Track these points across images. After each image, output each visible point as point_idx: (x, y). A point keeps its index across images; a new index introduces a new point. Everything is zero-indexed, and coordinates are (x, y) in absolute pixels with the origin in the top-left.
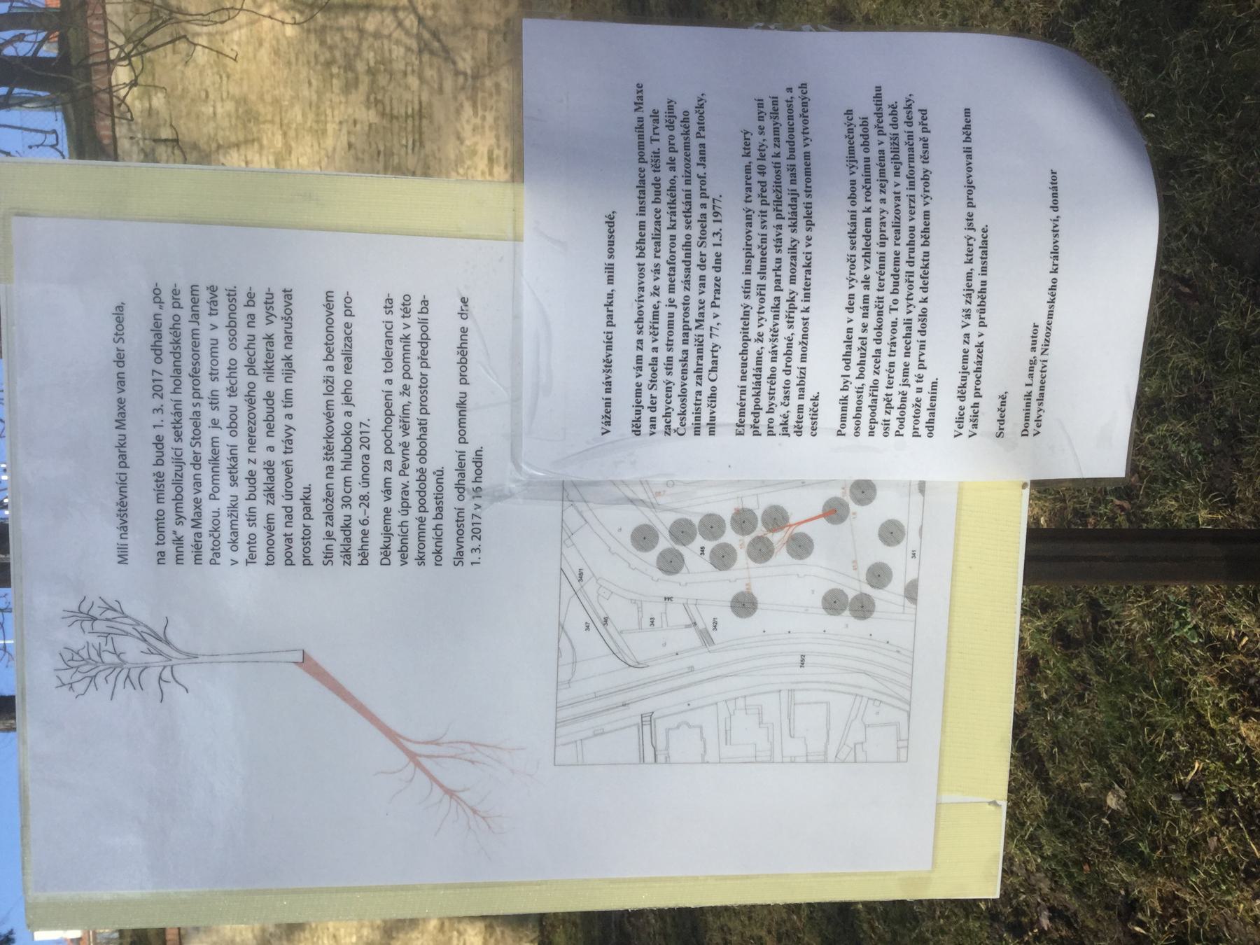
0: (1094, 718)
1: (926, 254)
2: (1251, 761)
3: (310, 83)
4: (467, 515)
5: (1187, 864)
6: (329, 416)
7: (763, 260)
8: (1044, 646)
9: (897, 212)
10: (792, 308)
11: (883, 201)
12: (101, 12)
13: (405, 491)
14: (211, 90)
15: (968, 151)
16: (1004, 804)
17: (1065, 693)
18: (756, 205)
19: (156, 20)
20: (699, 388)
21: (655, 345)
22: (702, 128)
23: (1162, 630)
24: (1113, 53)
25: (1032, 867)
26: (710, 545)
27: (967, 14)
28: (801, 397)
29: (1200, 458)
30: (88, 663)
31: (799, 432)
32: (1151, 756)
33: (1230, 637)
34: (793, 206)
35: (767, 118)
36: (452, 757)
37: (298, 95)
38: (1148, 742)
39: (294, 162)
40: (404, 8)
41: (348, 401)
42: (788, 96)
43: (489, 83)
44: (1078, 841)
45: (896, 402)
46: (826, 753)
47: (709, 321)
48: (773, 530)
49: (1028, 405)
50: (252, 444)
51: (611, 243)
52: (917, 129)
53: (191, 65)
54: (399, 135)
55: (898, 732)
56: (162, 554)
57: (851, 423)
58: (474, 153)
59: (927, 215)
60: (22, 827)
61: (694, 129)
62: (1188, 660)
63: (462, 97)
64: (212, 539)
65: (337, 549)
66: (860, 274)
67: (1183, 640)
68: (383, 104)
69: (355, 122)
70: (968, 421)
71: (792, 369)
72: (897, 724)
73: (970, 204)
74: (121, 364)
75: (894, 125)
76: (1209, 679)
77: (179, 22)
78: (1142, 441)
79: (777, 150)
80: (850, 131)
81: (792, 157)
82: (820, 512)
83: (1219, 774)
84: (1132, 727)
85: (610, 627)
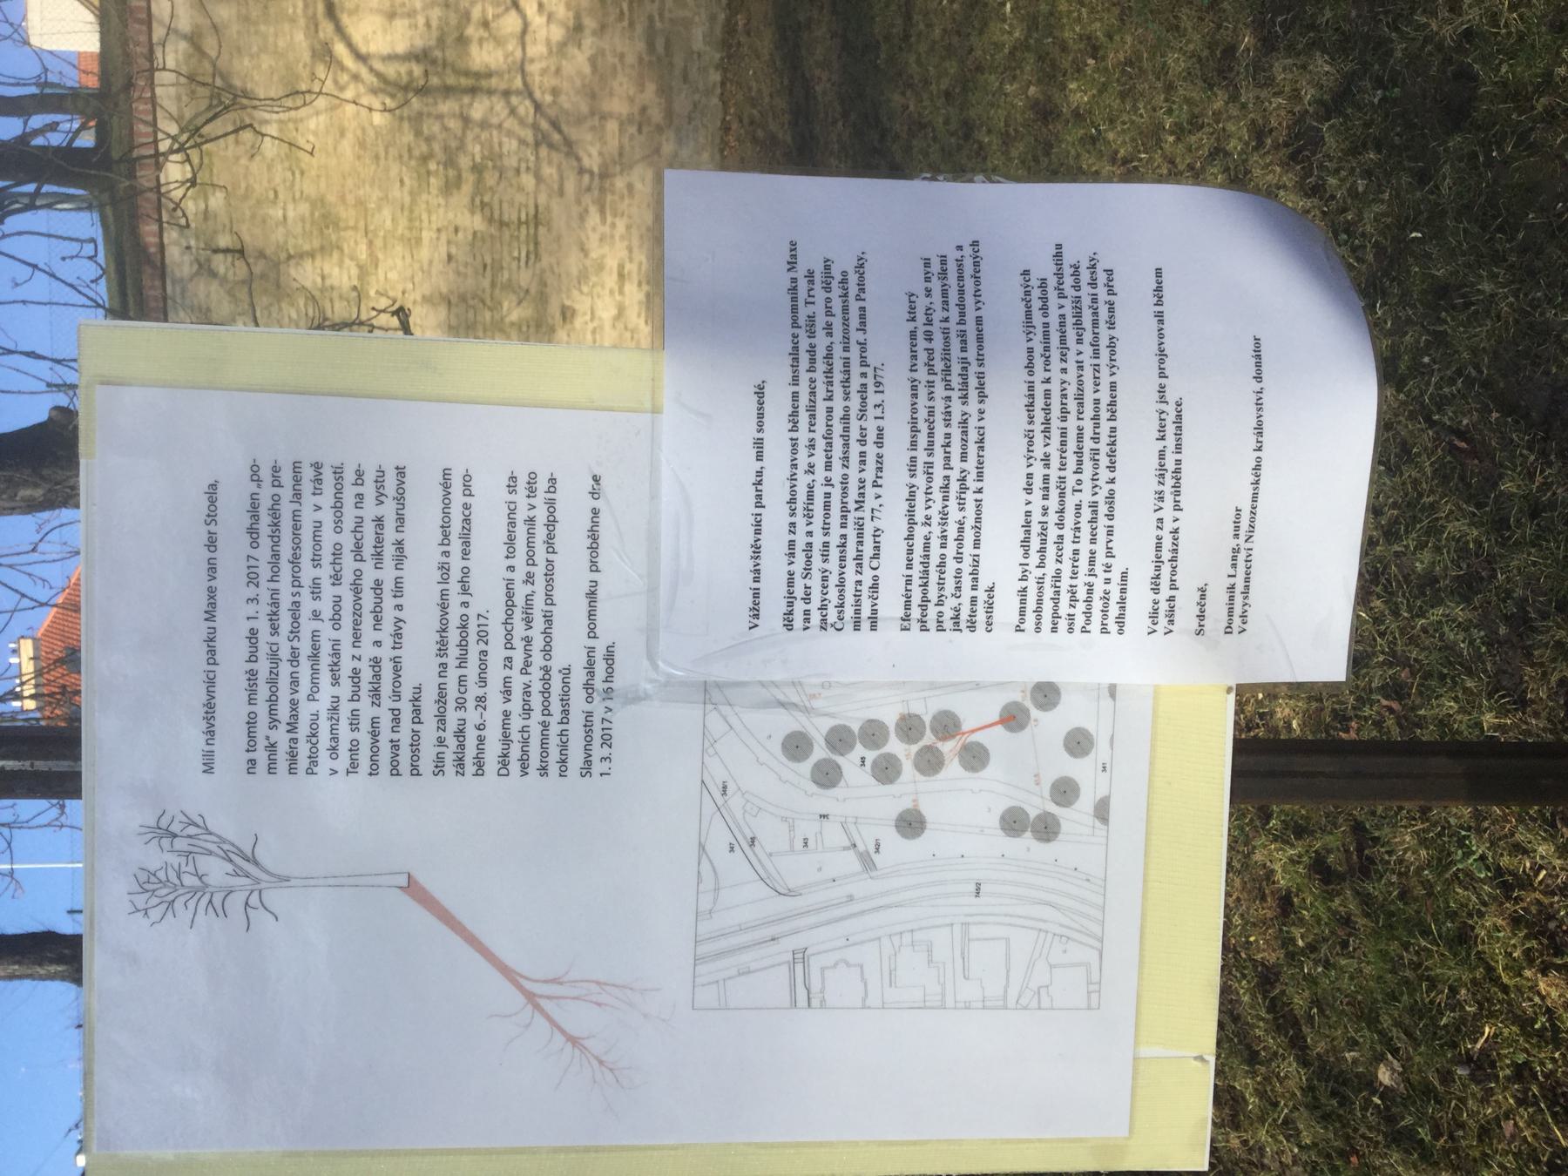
0: (1361, 971)
1: (1113, 429)
2: (1553, 1025)
3: (402, 181)
4: (596, 719)
5: (1477, 1154)
6: (444, 607)
7: (931, 435)
8: (1299, 881)
9: (1080, 383)
10: (964, 488)
11: (1064, 370)
12: (149, 95)
13: (527, 692)
14: (281, 190)
15: (1160, 317)
16: (1212, 1060)
17: (1325, 940)
18: (922, 374)
19: (217, 106)
20: (859, 577)
21: (809, 528)
22: (862, 290)
23: (1442, 862)
24: (1372, 160)
25: (1287, 1159)
26: (870, 756)
27: (1196, 111)
28: (974, 588)
29: (1484, 649)
30: (165, 886)
31: (972, 627)
32: (1431, 1018)
33: (1524, 871)
34: (964, 376)
35: (934, 279)
36: (574, 998)
37: (387, 196)
38: (1427, 1000)
39: (381, 276)
40: (518, 93)
41: (465, 590)
42: (958, 254)
43: (620, 183)
44: (1344, 1126)
45: (1082, 594)
46: (1005, 997)
47: (870, 502)
48: (944, 739)
49: (1232, 598)
50: (357, 638)
51: (761, 416)
52: (1102, 292)
53: (258, 158)
54: (510, 245)
55: (1089, 973)
56: (252, 762)
57: (1030, 618)
58: (600, 267)
59: (1113, 386)
60: (85, 1074)
61: (853, 290)
62: (1474, 898)
63: (587, 200)
64: (310, 745)
65: (449, 757)
66: (1039, 451)
67: (1469, 874)
68: (491, 209)
69: (456, 230)
70: (1163, 616)
71: (964, 556)
72: (1088, 965)
73: (1162, 375)
74: (212, 549)
75: (1077, 287)
76: (1500, 922)
77: (244, 108)
78: (1413, 628)
79: (945, 314)
80: (1027, 293)
81: (962, 322)
82: (997, 718)
83: (1513, 1041)
84: (1407, 982)
85: (757, 848)
